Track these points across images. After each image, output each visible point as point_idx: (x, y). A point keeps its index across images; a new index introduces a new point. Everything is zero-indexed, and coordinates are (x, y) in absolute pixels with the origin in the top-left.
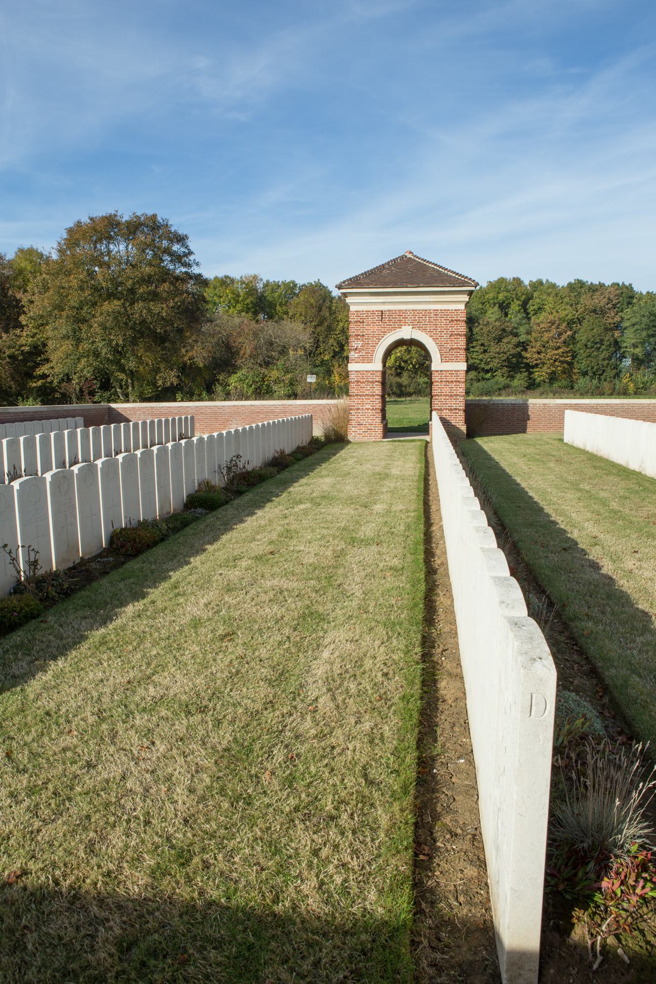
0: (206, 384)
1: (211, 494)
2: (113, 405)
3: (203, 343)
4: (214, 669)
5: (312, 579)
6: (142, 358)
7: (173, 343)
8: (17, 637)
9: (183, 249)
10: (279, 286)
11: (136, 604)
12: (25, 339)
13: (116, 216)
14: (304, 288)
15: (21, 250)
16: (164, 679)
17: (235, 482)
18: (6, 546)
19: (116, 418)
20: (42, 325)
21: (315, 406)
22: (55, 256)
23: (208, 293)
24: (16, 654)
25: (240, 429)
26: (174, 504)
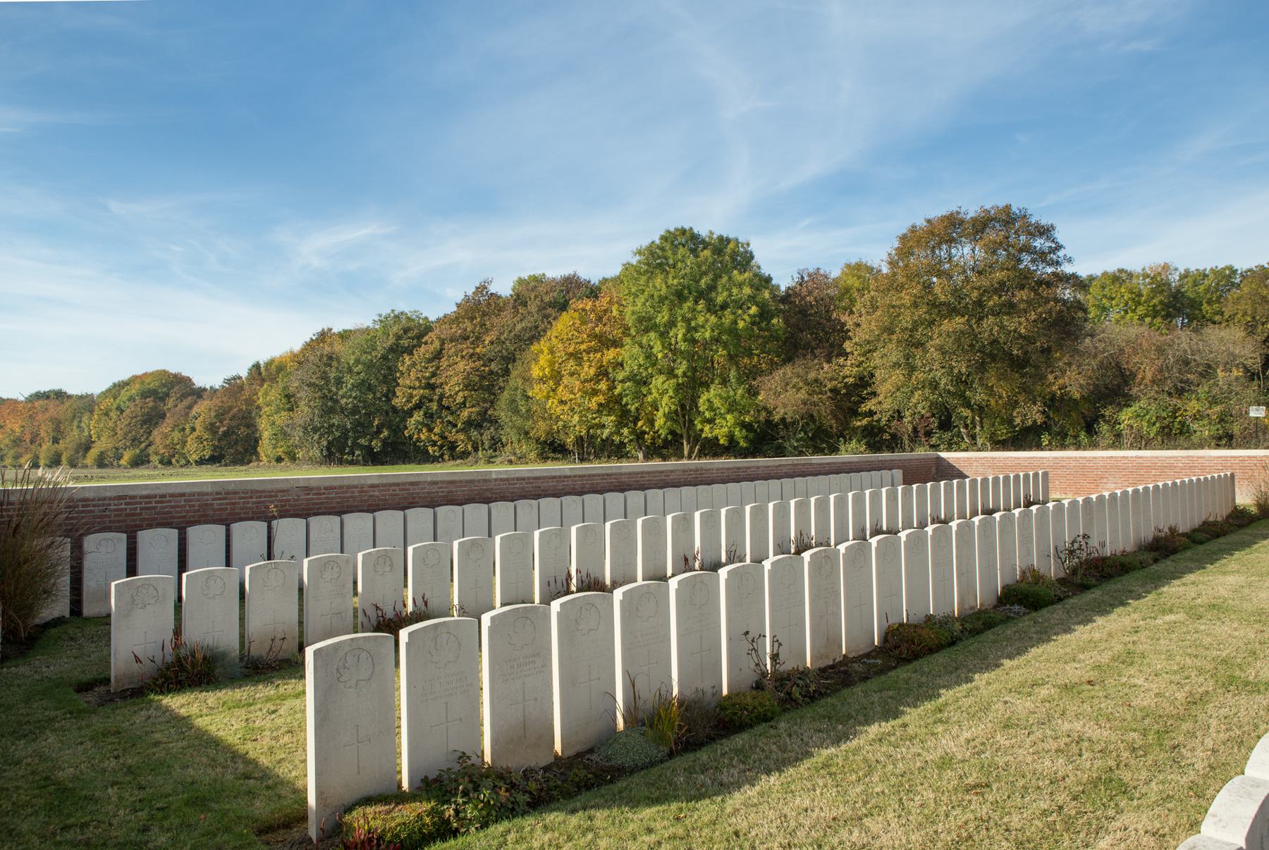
0: (1086, 421)
1: (1036, 588)
2: (944, 455)
3: (1079, 366)
4: (940, 827)
5: (1135, 731)
6: (995, 389)
7: (1037, 367)
8: (740, 740)
9: (1048, 244)
10: (1205, 276)
11: (883, 724)
12: (849, 369)
13: (958, 213)
14: (1249, 275)
15: (848, 266)
16: (874, 825)
17: (1080, 572)
18: (747, 633)
19: (946, 472)
20: (870, 351)
21: (1243, 459)
22: (885, 270)
23: (1089, 299)
24: (732, 759)
25: (1170, 483)
26: (980, 598)
